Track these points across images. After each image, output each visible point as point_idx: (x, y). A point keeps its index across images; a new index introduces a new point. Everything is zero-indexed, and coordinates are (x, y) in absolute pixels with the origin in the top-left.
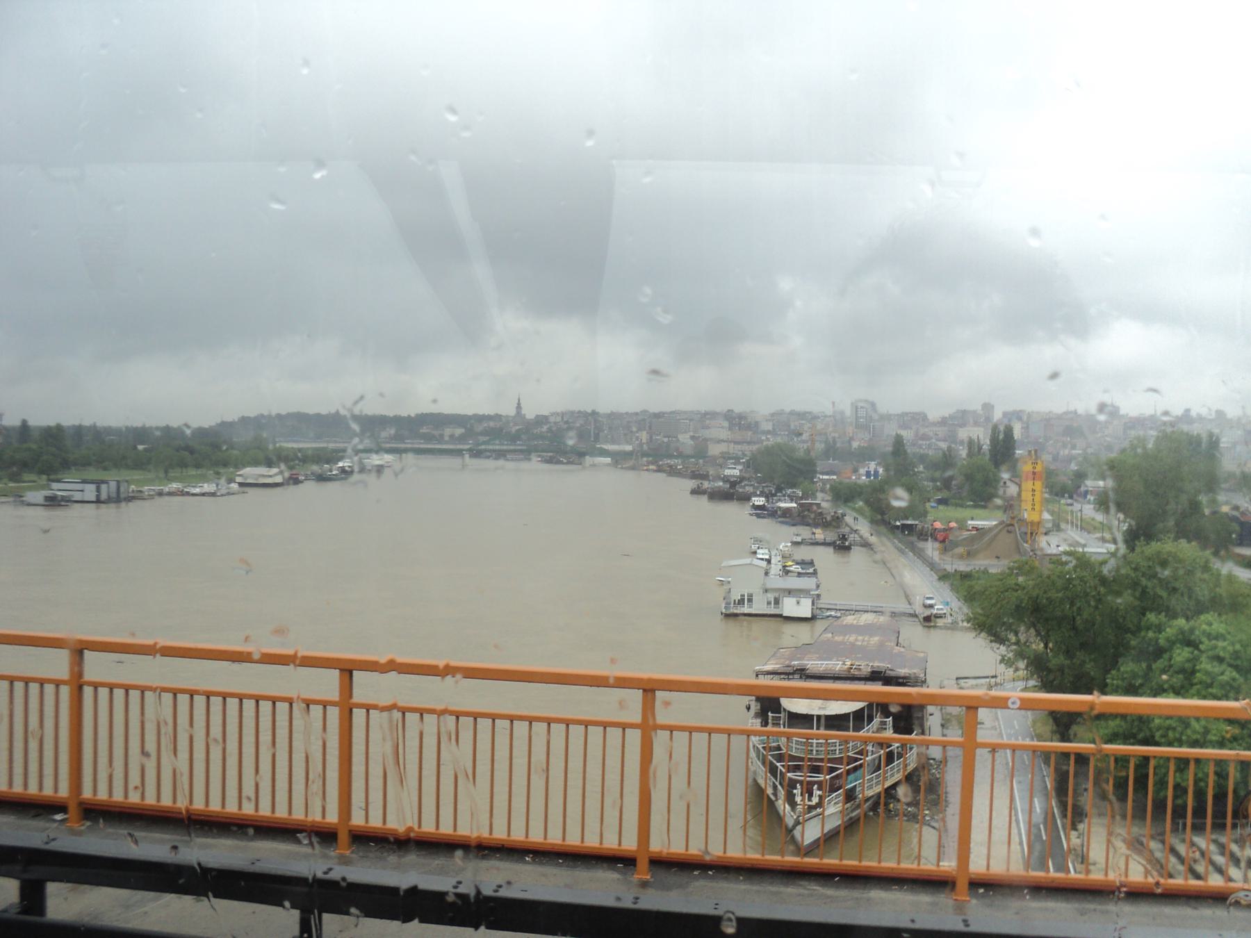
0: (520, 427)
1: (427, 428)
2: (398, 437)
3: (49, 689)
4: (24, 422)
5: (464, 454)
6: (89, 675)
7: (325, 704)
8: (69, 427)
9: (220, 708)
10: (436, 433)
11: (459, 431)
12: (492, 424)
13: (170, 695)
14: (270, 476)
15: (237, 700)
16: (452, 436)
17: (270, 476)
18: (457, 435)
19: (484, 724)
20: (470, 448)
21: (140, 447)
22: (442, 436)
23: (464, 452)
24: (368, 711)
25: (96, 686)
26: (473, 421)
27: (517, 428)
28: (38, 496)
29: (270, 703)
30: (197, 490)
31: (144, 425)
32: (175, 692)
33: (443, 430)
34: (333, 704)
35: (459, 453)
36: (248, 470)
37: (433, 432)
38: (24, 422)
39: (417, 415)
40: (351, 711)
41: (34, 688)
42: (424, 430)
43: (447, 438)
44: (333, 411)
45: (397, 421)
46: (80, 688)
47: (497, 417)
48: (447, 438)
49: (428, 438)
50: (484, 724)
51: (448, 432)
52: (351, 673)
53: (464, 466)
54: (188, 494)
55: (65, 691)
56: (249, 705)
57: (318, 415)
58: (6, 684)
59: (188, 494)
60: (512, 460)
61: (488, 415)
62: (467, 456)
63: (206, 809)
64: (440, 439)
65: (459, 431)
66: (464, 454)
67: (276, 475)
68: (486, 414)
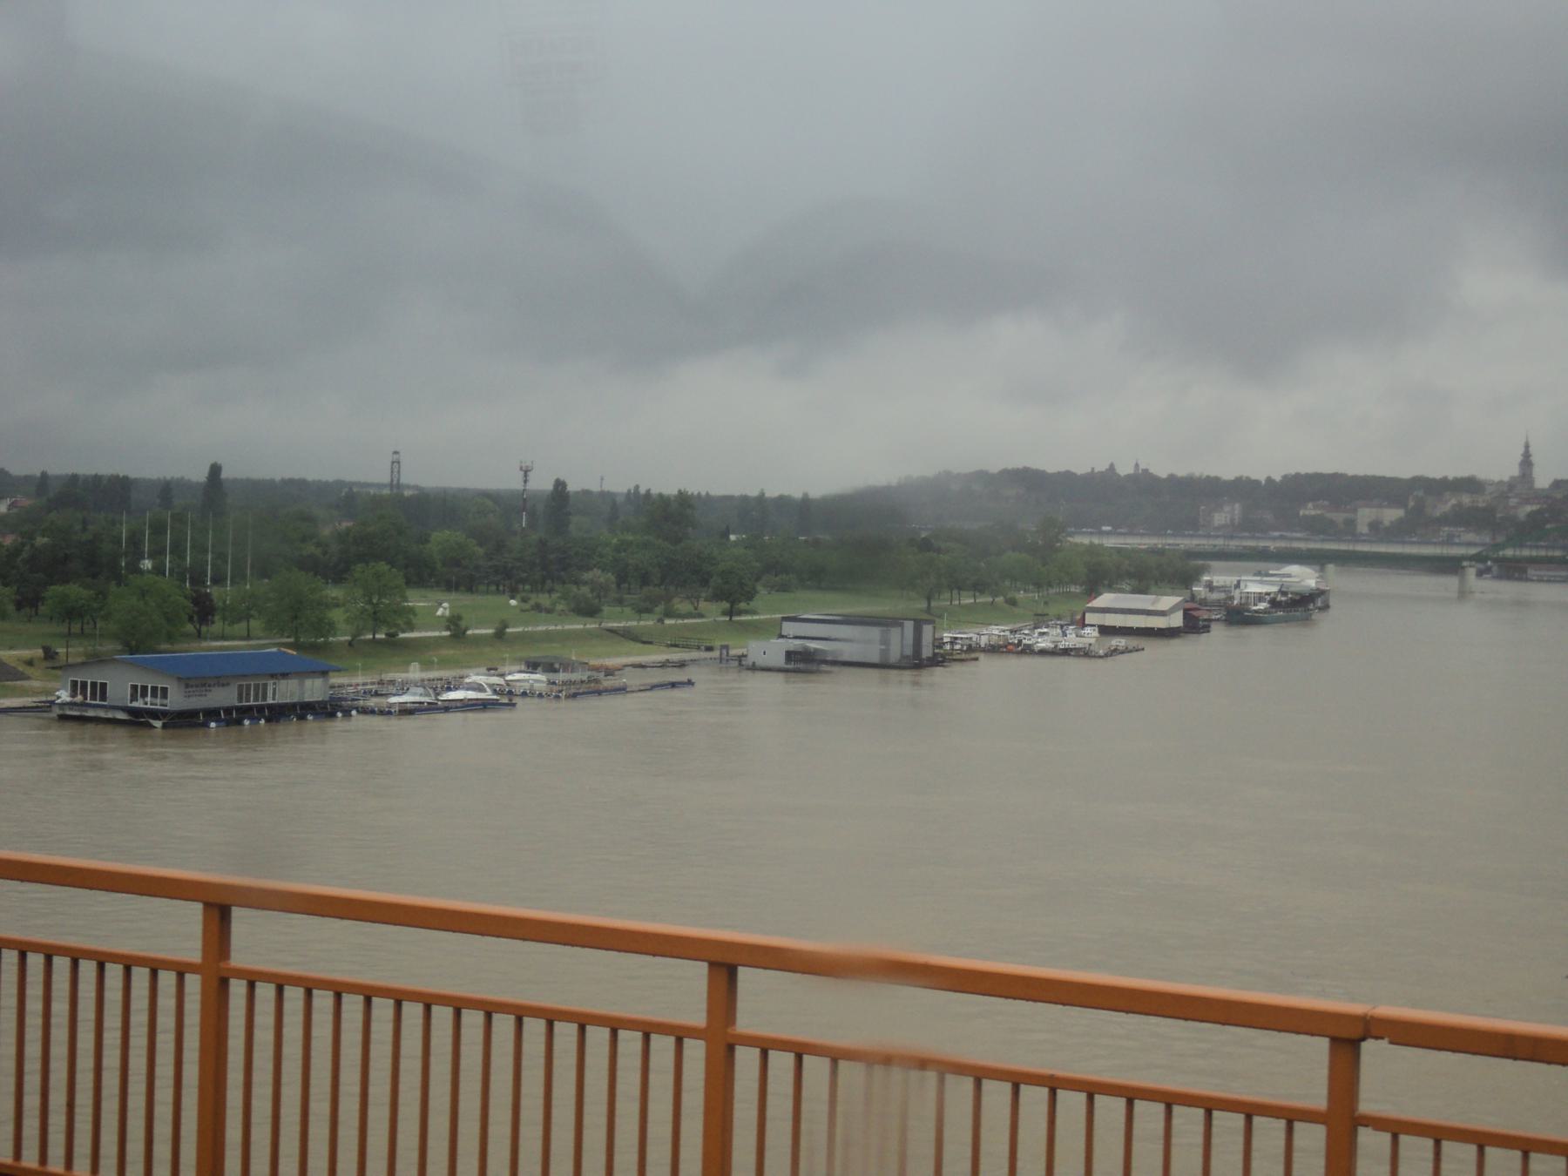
0: (1535, 508)
1: (1315, 507)
2: (1249, 526)
3: (167, 979)
4: (560, 485)
5: (1463, 568)
6: (747, 1021)
7: (1292, 1117)
8: (58, 477)
9: (606, 1049)
10: (1339, 517)
11: (1391, 515)
12: (1466, 500)
13: (968, 1083)
14: (1162, 613)
15: (1044, 1092)
16: (1375, 526)
17: (1162, 613)
18: (1387, 523)
19: (1149, 1115)
20: (1479, 553)
21: (733, 537)
22: (1351, 523)
23: (1465, 564)
24: (1209, 1113)
25: (766, 1048)
26: (1420, 493)
27: (1529, 508)
28: (771, 650)
29: (1007, 1087)
30: (1043, 644)
31: (806, 495)
32: (253, 978)
33: (1355, 511)
34: (1309, 1116)
35: (1449, 566)
36: (1105, 599)
37: (1329, 515)
38: (560, 485)
39: (1285, 477)
40: (731, 1049)
41: (141, 976)
42: (1309, 510)
43: (1363, 528)
44: (1101, 467)
45: (1242, 489)
46: (224, 983)
47: (1470, 485)
48: (1363, 528)
49: (1317, 527)
50: (1149, 1115)
51: (1365, 515)
52: (731, 972)
53: (1463, 594)
54: (1028, 651)
55: (695, 1051)
56: (630, 1042)
57: (1068, 476)
58: (11, 957)
59: (1028, 651)
60: (1540, 580)
61: (1172, 477)
62: (1471, 573)
63: (16, 1164)
64: (1349, 531)
65: (1391, 515)
66: (1463, 568)
67: (1173, 610)
68: (1125, 469)
